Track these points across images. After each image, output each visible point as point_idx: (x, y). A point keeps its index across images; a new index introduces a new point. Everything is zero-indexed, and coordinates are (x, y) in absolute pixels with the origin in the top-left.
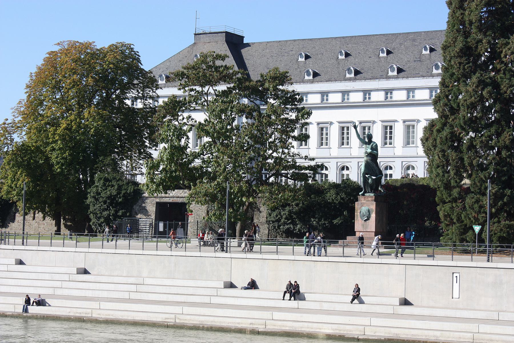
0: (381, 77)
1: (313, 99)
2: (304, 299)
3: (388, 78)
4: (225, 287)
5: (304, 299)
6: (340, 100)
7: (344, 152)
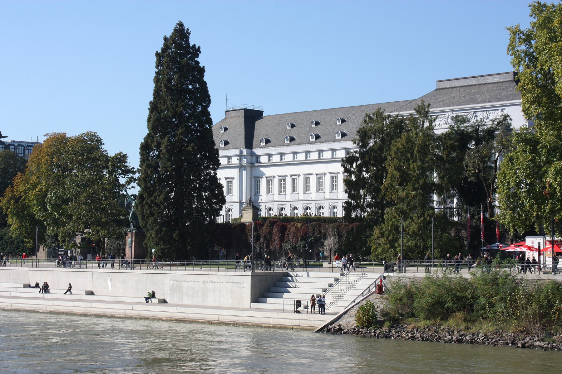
0: (279, 146)
1: (264, 160)
2: (49, 293)
3: (335, 141)
4: (86, 294)
5: (49, 293)
6: (304, 159)
7: (333, 195)
